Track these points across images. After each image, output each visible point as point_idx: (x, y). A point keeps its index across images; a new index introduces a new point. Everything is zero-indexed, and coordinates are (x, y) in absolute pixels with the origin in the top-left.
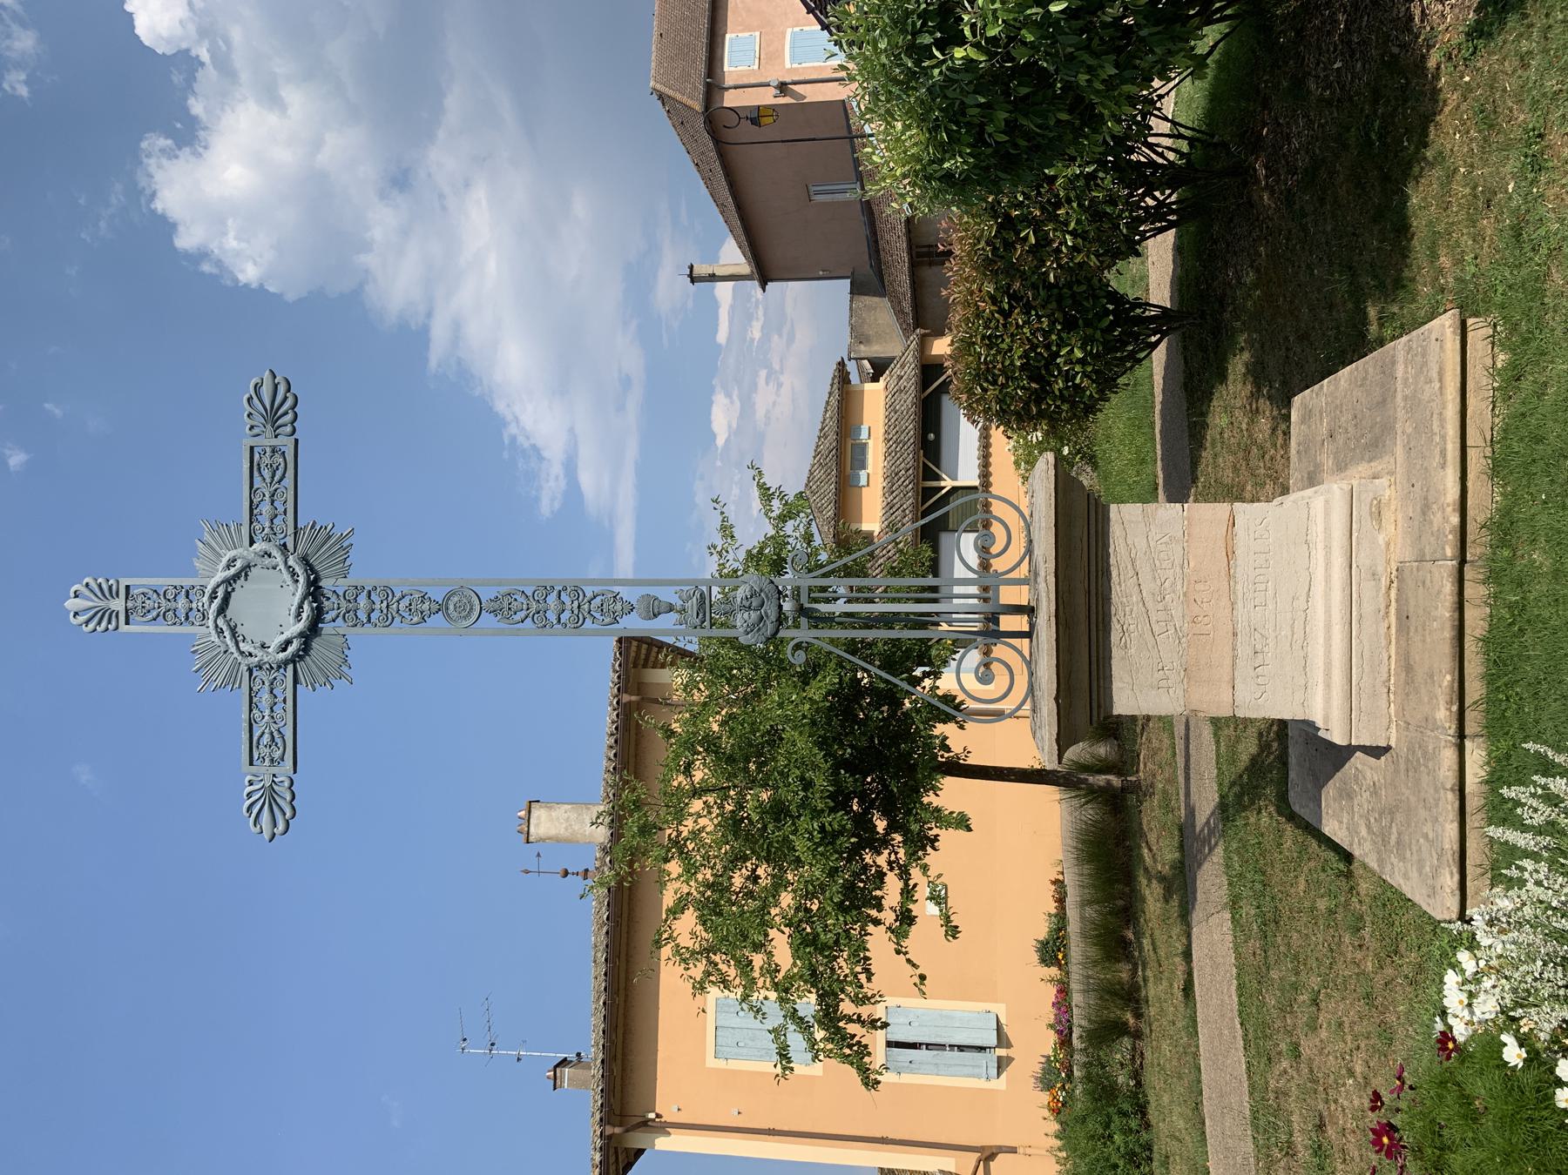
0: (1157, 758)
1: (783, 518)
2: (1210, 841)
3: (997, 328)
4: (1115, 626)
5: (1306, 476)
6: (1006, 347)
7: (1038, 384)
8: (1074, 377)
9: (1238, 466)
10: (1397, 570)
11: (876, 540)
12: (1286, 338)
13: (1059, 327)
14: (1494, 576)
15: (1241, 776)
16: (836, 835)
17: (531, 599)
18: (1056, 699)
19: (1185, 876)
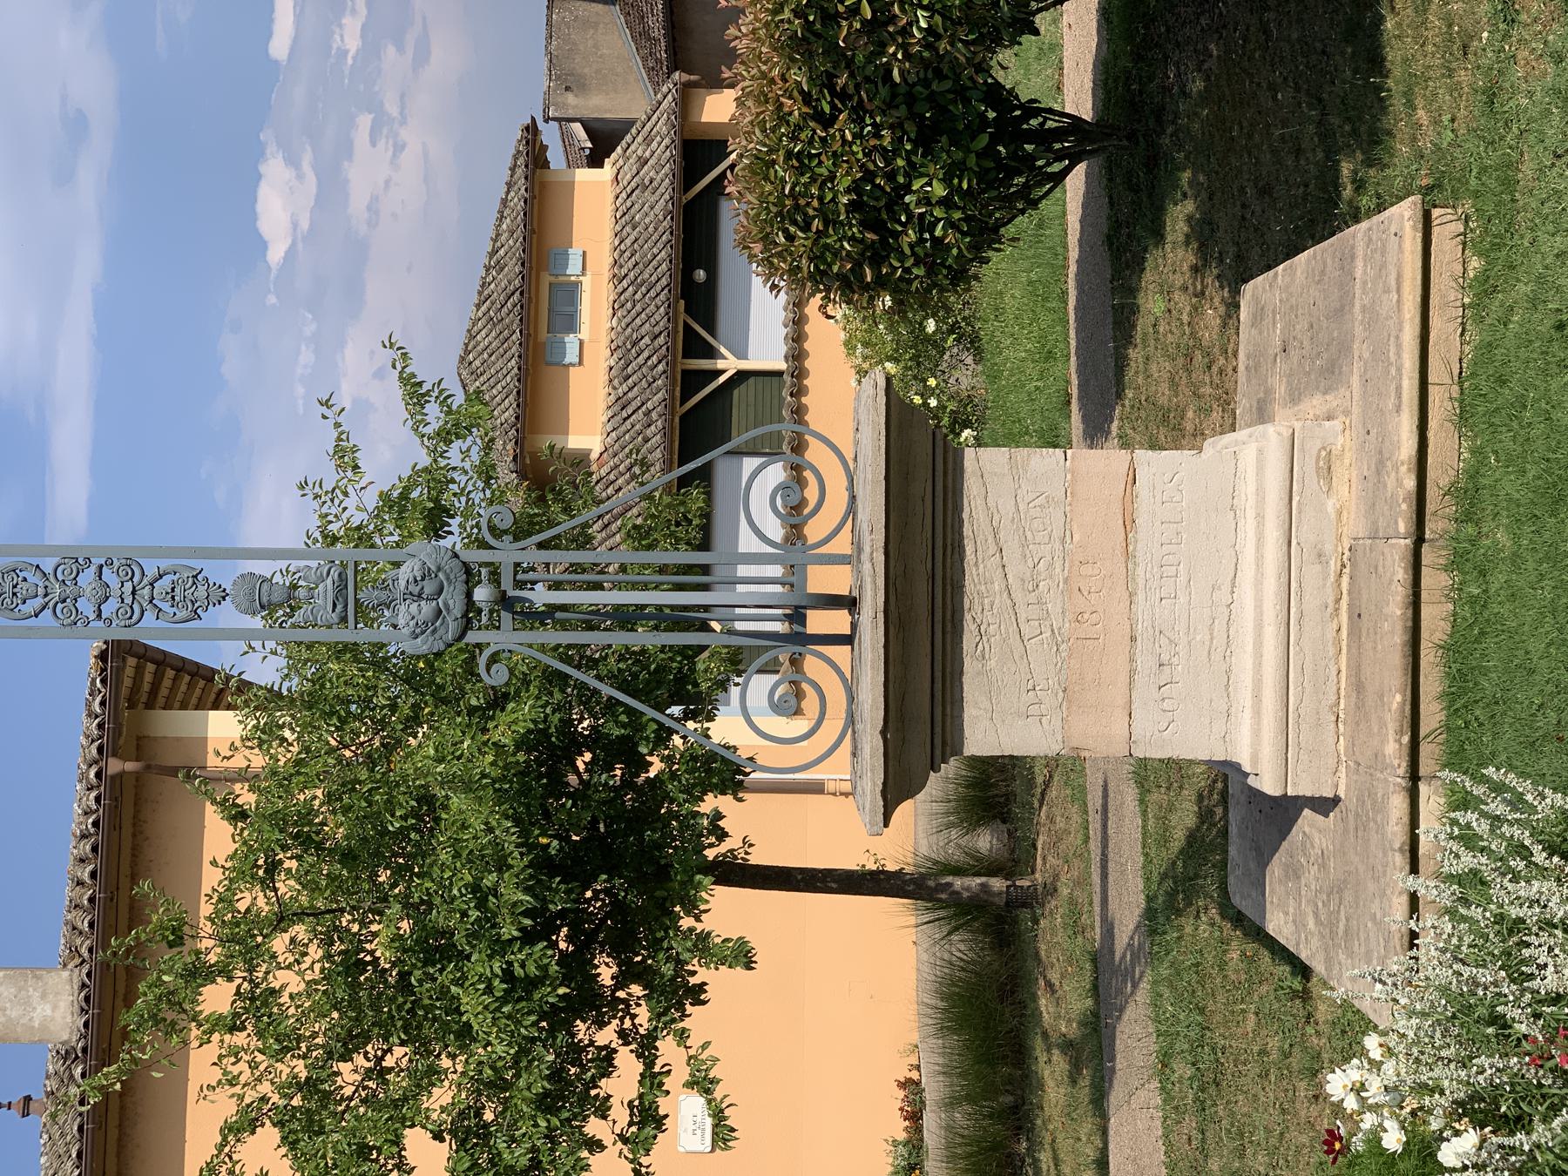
0: (1063, 847)
1: (446, 436)
2: (1134, 971)
3: (811, 142)
4: (969, 628)
5: (1255, 404)
6: (826, 173)
7: (875, 233)
8: (933, 225)
9: (1177, 379)
10: (1350, 550)
11: (594, 467)
12: (1242, 189)
13: (908, 147)
14: (1457, 562)
15: (1174, 863)
16: (532, 984)
17: (52, 578)
18: (883, 733)
19: (1099, 1037)
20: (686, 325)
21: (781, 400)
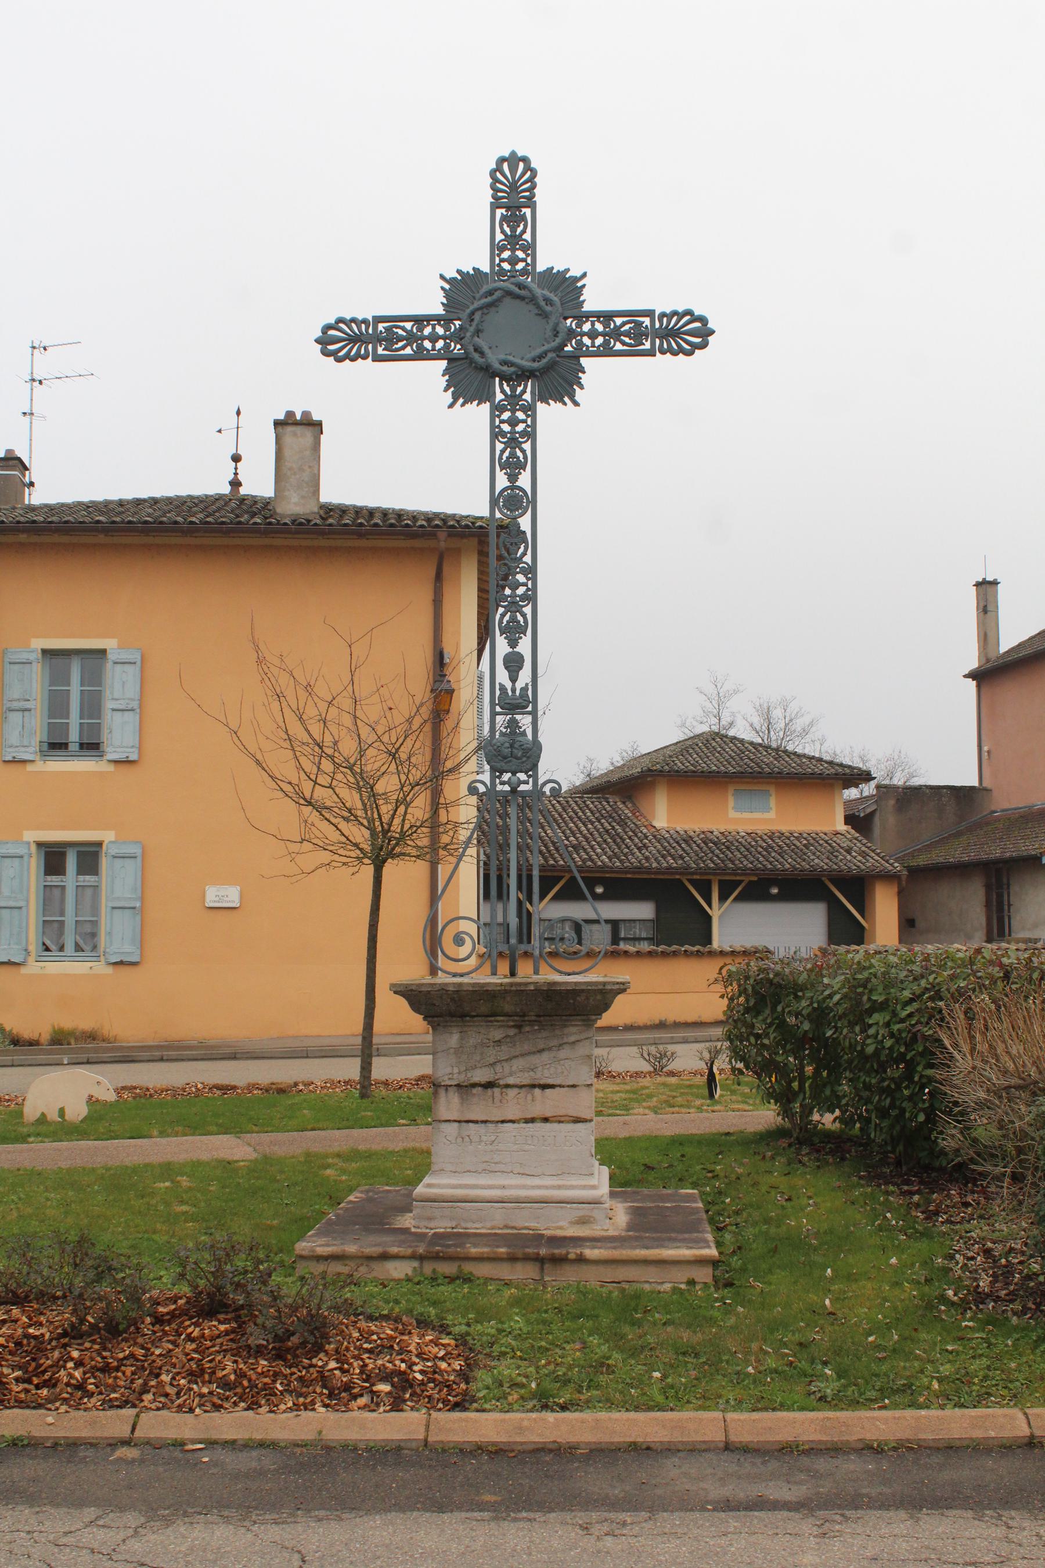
20: (741, 882)
21: (682, 946)
